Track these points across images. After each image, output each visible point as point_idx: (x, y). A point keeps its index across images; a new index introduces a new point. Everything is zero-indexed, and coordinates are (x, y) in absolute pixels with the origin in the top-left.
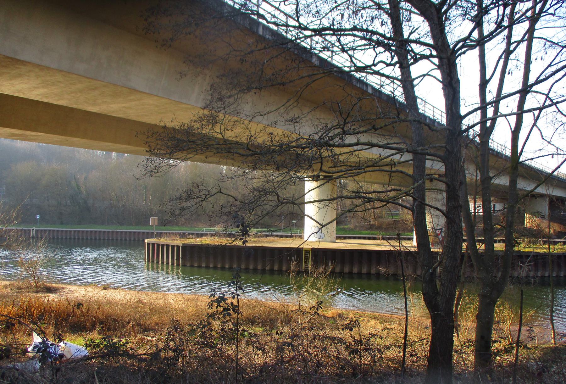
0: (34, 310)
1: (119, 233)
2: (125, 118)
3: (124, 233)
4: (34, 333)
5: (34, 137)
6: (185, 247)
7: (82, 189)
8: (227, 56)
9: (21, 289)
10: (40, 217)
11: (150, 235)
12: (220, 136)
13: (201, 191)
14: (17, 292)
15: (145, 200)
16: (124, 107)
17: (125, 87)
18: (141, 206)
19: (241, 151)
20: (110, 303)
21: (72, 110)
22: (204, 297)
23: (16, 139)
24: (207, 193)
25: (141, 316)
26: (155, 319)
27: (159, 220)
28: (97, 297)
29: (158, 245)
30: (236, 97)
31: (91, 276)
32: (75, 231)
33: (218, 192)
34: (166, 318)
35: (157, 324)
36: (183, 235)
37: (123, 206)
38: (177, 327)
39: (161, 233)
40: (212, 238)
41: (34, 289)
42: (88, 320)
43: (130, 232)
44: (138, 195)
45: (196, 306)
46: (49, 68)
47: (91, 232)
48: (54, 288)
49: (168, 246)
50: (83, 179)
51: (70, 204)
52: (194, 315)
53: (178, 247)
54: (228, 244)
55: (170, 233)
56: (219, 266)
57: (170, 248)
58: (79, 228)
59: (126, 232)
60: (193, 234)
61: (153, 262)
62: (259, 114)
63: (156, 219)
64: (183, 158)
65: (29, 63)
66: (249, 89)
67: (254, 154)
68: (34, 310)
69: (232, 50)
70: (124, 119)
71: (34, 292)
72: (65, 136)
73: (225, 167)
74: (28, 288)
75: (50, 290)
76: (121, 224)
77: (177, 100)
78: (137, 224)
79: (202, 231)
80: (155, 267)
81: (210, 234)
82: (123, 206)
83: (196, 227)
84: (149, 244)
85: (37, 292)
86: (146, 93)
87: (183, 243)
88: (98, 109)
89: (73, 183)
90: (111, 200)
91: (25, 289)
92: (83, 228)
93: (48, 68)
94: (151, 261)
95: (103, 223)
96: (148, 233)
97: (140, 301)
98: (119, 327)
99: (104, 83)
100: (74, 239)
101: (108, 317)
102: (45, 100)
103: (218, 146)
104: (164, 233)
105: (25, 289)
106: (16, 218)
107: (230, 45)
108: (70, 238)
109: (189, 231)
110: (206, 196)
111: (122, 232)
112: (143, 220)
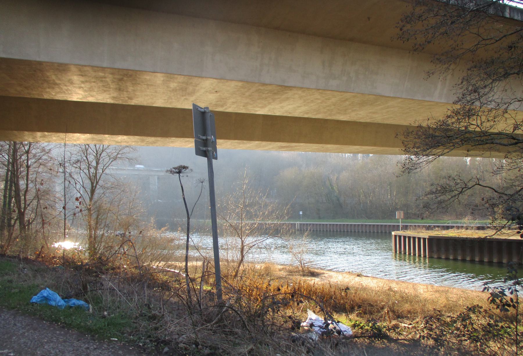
0: (304, 291)
1: (376, 226)
2: (371, 122)
3: (372, 226)
4: (308, 310)
5: (298, 147)
6: (431, 240)
7: (334, 188)
8: (476, 47)
9: (291, 272)
10: (303, 213)
11: (397, 228)
12: (478, 129)
13: (457, 184)
14: (289, 275)
15: (390, 195)
16: (370, 113)
17: (371, 95)
18: (386, 201)
19: (505, 141)
20: (364, 289)
21: (326, 121)
22: (454, 290)
23: (284, 151)
24: (463, 186)
25: (394, 304)
26: (407, 307)
27: (404, 213)
28: (353, 282)
29: (405, 237)
30: (491, 86)
31: (410, 271)
32: (330, 225)
33: (476, 184)
34: (418, 307)
35: (409, 312)
36: (429, 228)
37: (371, 201)
38: (155, 283)
39: (407, 226)
40: (460, 231)
41: (301, 273)
42: (346, 302)
43: (378, 225)
44: (383, 191)
45: (447, 298)
46: (309, 88)
47: (344, 225)
48: (317, 273)
49: (414, 238)
50: (335, 180)
51: (325, 201)
52: (444, 307)
53: (424, 239)
54: (488, 237)
55: (415, 226)
56: (468, 259)
57: (417, 240)
58: (334, 222)
59: (374, 225)
60: (438, 227)
61: (400, 253)
62: (516, 100)
63: (402, 213)
64: (440, 154)
65: (295, 87)
66: (506, 75)
67: (516, 143)
68: (304, 291)
69: (481, 39)
70: (370, 123)
71: (301, 275)
72: (321, 144)
73: (468, 159)
74: (296, 272)
75: (313, 274)
76: (369, 218)
77: (420, 99)
78: (383, 218)
79: (448, 224)
80: (417, 260)
81: (456, 226)
82: (371, 201)
83: (441, 220)
84: (395, 236)
85: (304, 275)
86: (390, 97)
87: (429, 235)
88: (349, 118)
89: (327, 183)
90: (359, 196)
91: (294, 272)
92: (337, 222)
93: (308, 89)
94: (398, 252)
95: (353, 217)
96: (394, 226)
97: (390, 289)
98: (374, 312)
99: (353, 94)
100: (330, 231)
101: (364, 301)
102: (306, 116)
103: (479, 138)
104: (410, 226)
105: (294, 272)
106: (288, 214)
107: (478, 35)
108: (327, 231)
109: (433, 223)
110: (463, 188)
111: (370, 225)
112: (390, 214)
